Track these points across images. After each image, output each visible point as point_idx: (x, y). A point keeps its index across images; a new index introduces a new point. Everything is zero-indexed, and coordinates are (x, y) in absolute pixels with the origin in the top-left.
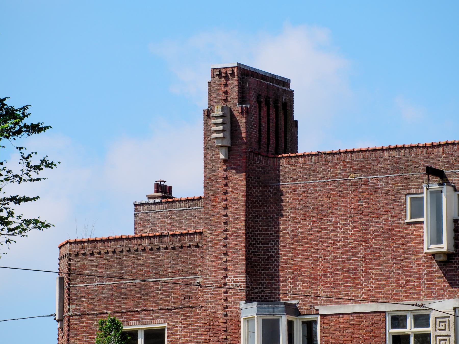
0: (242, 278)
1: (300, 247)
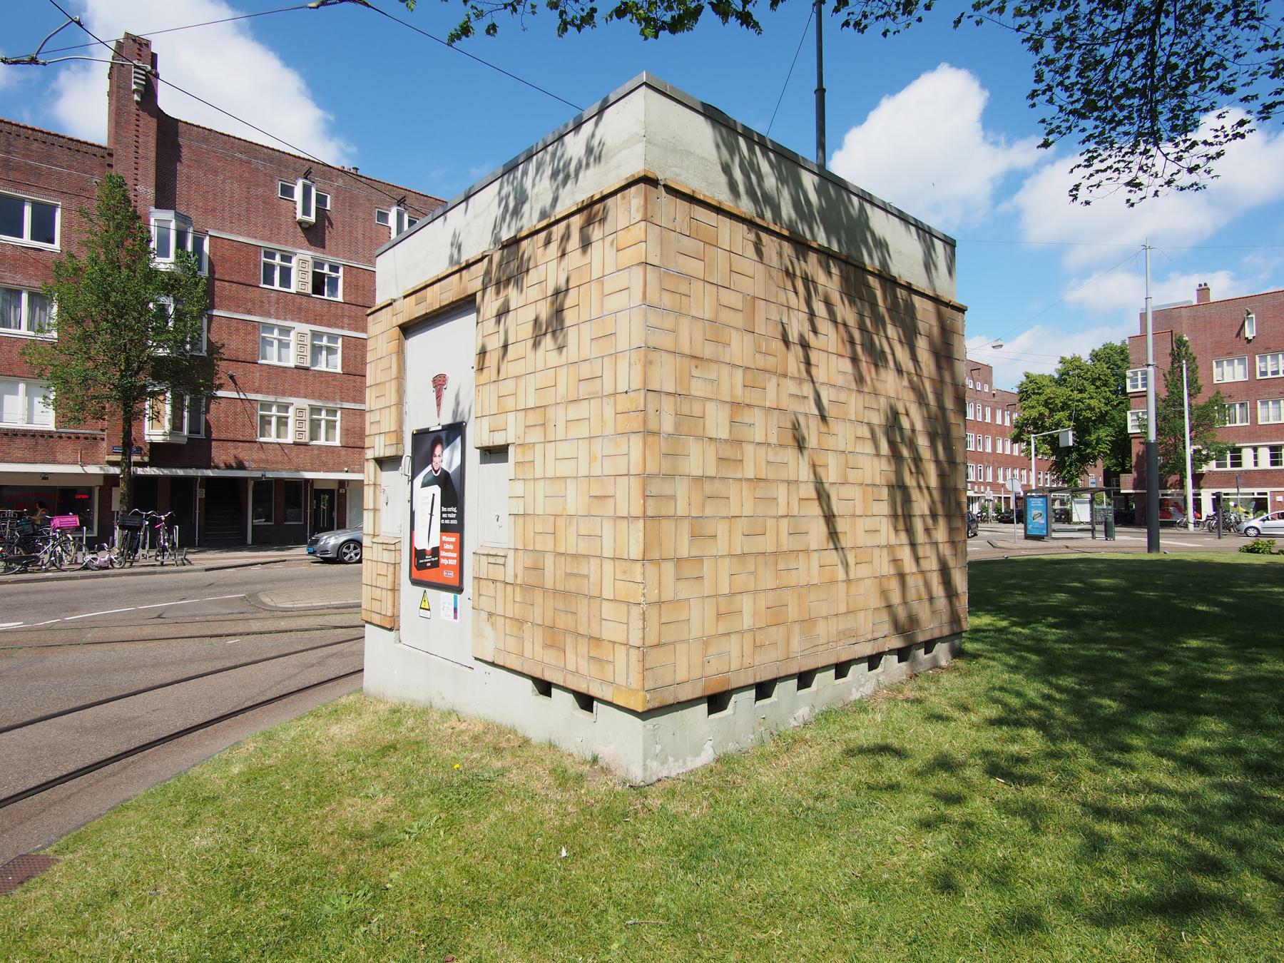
1: (194, 187)
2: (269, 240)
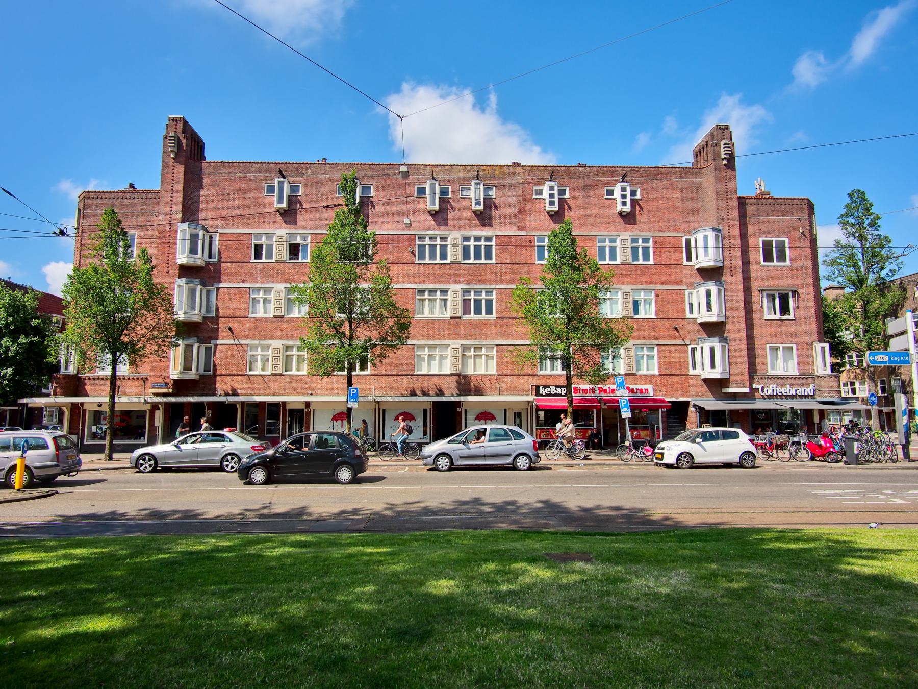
0: (180, 212)
1: (210, 203)
2: (257, 227)
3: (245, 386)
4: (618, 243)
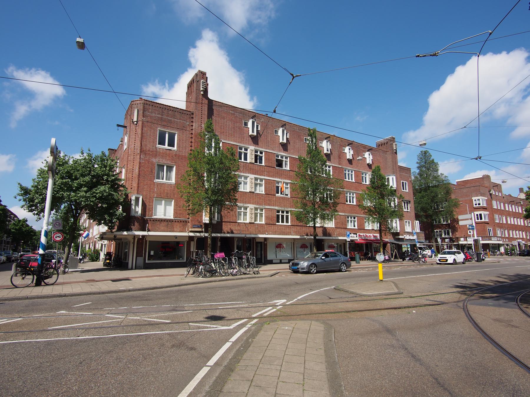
2: (241, 143)
3: (237, 229)
4: (249, 152)
